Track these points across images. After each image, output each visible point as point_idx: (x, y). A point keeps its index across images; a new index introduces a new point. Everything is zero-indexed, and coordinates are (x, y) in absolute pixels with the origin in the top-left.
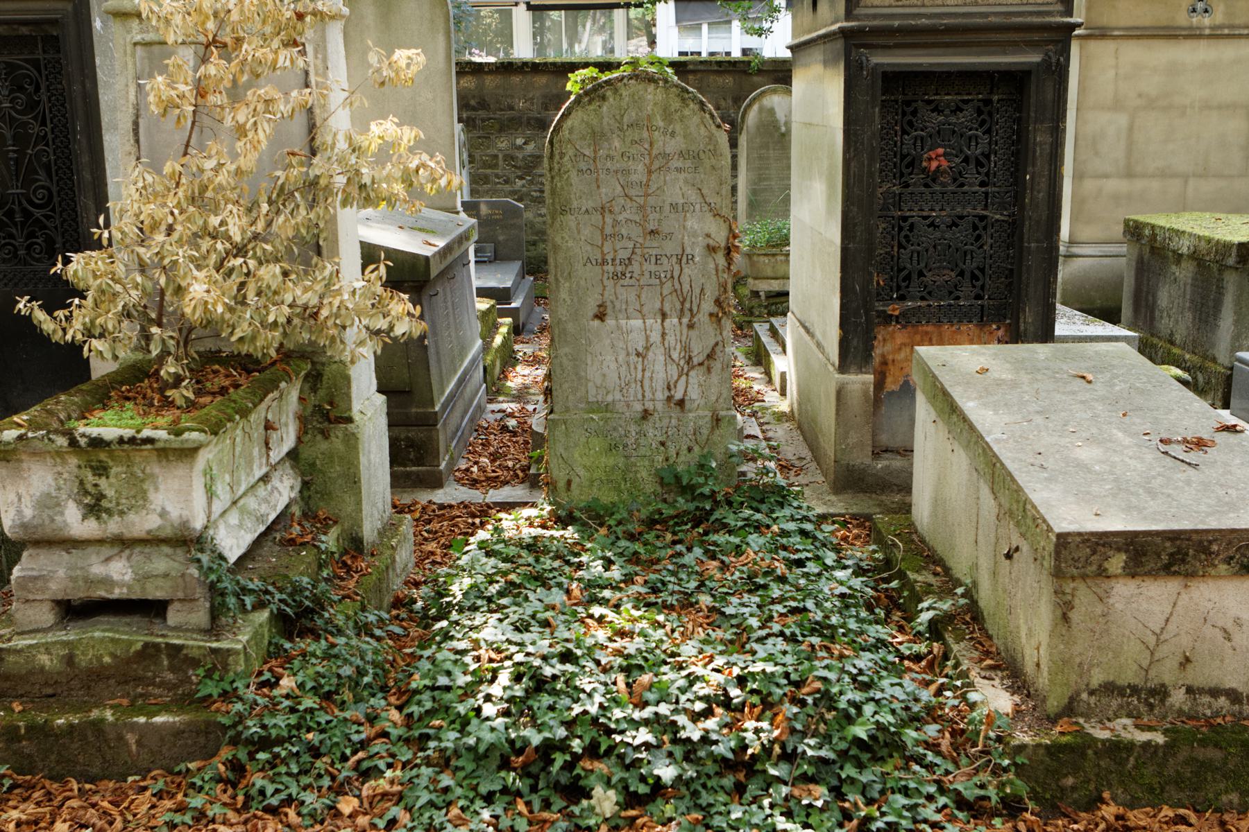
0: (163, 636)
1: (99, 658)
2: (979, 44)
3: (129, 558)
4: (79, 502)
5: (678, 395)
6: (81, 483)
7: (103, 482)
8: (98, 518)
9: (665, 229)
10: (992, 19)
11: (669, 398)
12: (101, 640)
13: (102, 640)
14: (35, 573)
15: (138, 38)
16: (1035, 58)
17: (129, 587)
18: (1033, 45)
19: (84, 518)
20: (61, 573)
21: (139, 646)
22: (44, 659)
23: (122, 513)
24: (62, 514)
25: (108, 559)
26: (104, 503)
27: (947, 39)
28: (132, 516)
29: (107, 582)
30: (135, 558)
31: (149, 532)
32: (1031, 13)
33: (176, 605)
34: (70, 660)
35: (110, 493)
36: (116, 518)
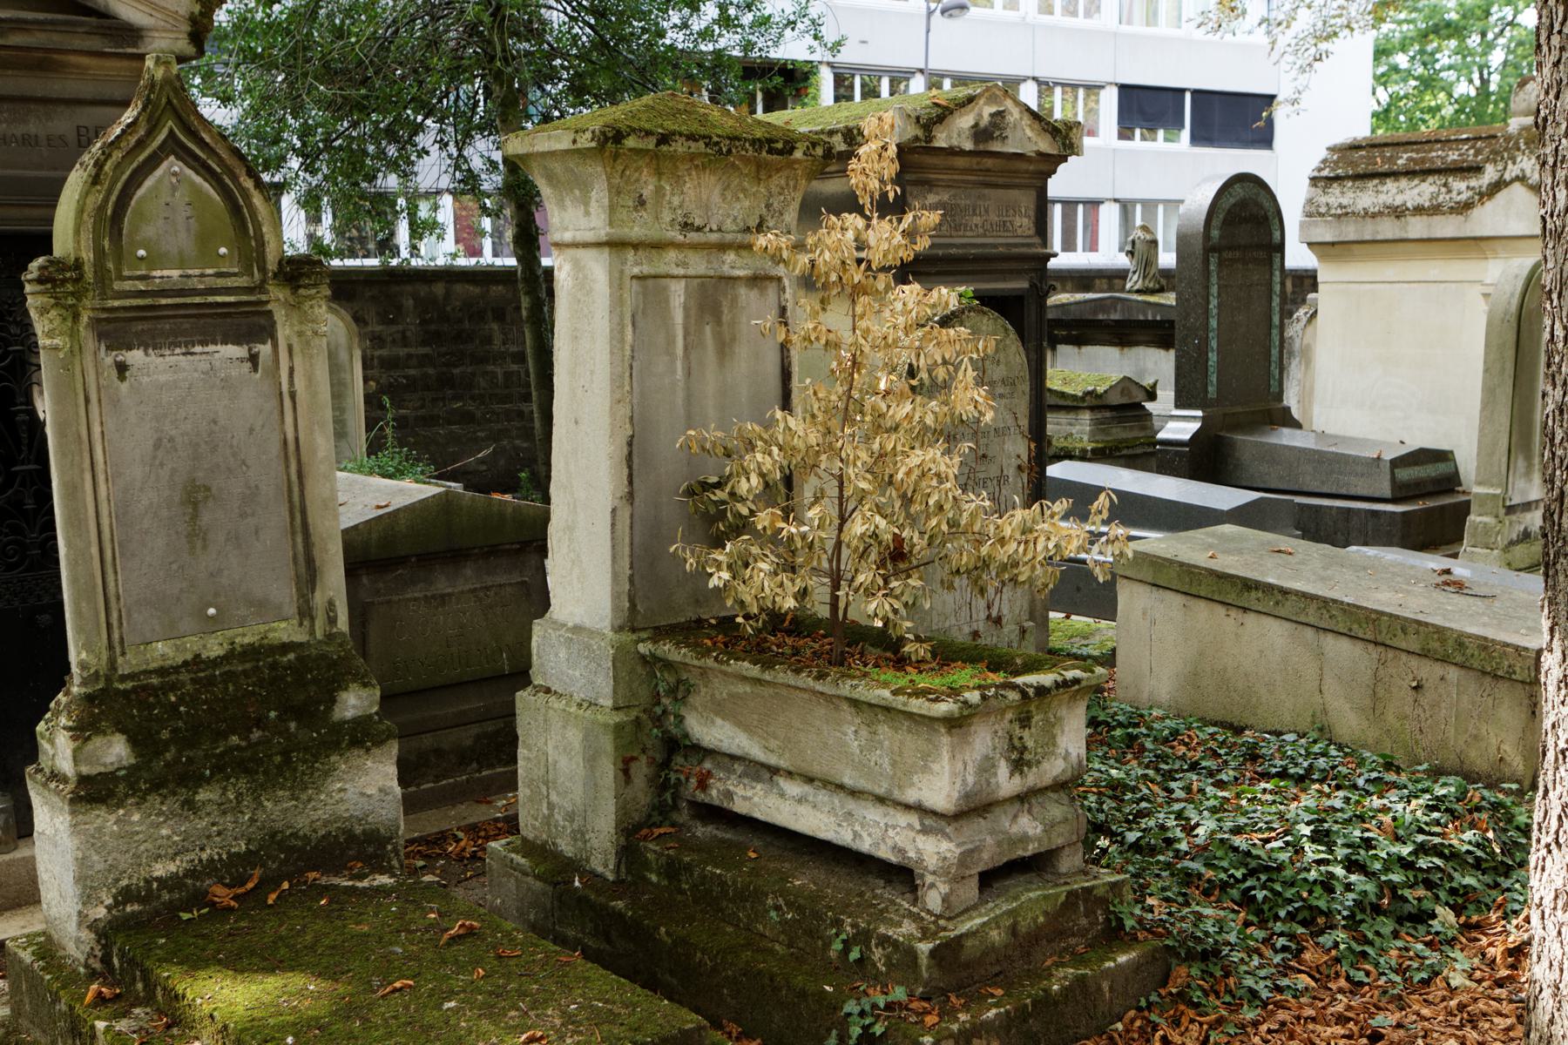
0: (1066, 883)
1: (1035, 919)
2: (990, 272)
3: (1029, 812)
4: (1008, 759)
5: (994, 614)
6: (1011, 739)
7: (1026, 734)
8: (1021, 773)
9: (990, 454)
10: (953, 251)
11: (989, 617)
12: (1031, 900)
13: (1037, 899)
14: (970, 846)
15: (636, 270)
16: (1025, 285)
17: (1039, 840)
18: (1017, 273)
19: (1012, 775)
20: (989, 840)
21: (1063, 897)
22: (995, 936)
23: (1039, 762)
24: (995, 774)
25: (1015, 817)
26: (1027, 756)
27: (1005, 266)
28: (1045, 765)
29: (1024, 839)
30: (1035, 810)
31: (1055, 779)
32: (1023, 245)
33: (1067, 851)
34: (1013, 930)
35: (1030, 744)
36: (1034, 769)
